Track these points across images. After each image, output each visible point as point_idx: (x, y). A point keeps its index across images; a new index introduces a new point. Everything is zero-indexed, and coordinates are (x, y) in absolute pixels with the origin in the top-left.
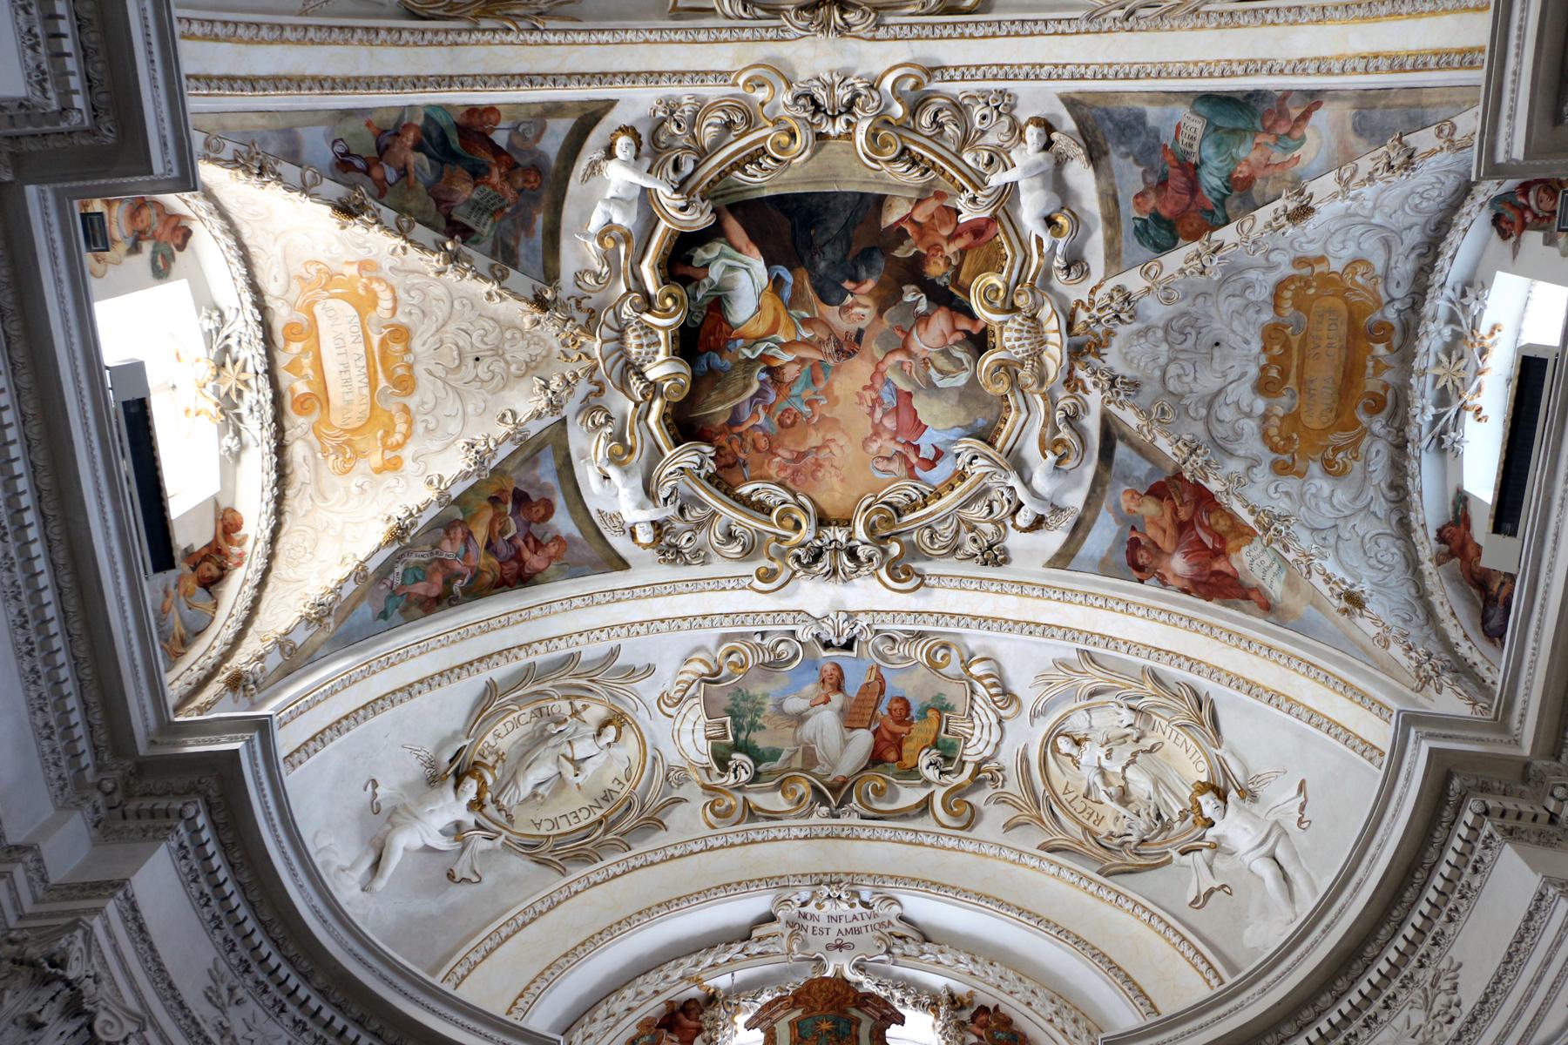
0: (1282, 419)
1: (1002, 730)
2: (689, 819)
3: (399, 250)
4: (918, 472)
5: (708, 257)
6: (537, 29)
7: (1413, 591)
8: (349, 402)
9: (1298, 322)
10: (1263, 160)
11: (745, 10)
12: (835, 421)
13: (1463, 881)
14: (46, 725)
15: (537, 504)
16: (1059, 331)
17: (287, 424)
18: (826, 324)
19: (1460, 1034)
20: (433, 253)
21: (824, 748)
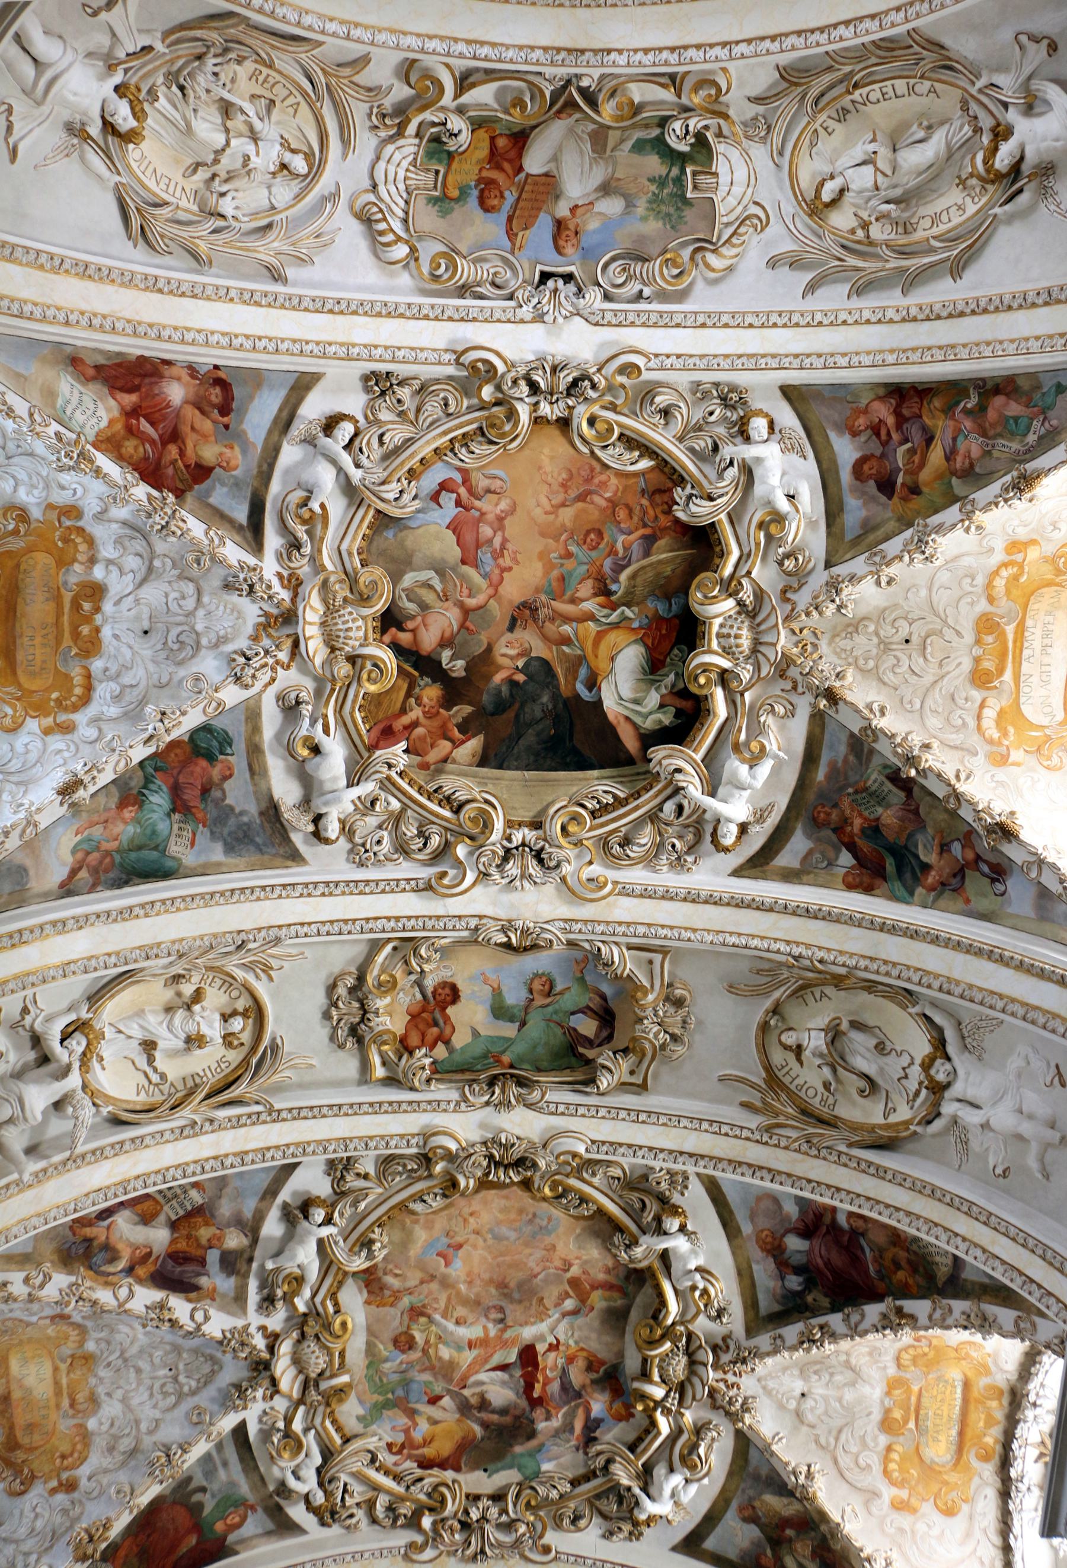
0: (74, 560)
1: (372, 177)
3: (963, 776)
4: (458, 477)
5: (659, 716)
6: (794, 957)
8: (1049, 613)
9: (66, 660)
10: (110, 826)
11: (599, 949)
12: (543, 535)
15: (870, 477)
16: (306, 640)
18: (545, 638)
20: (930, 768)
21: (581, 152)
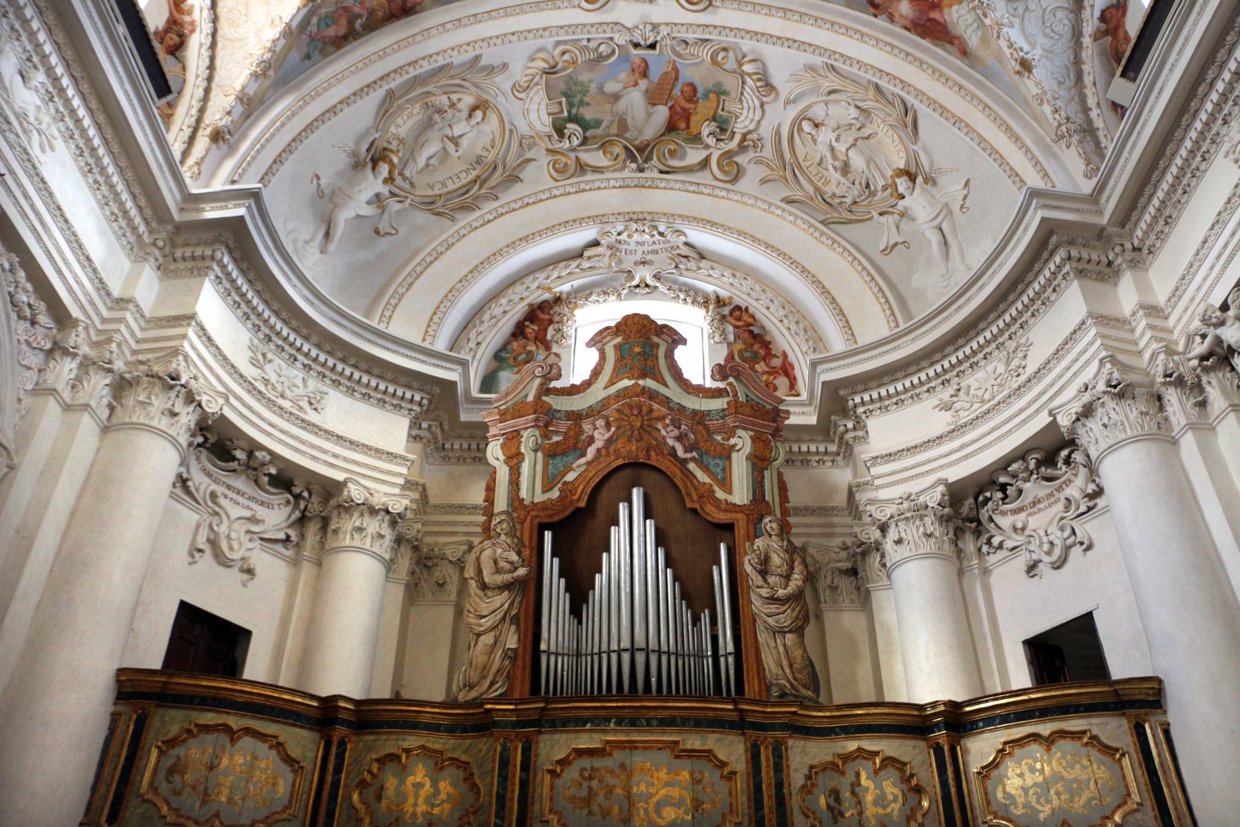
1: (763, 111)
2: (538, 174)
7: (1072, 57)
13: (1046, 295)
14: (112, 213)
19: (1020, 387)
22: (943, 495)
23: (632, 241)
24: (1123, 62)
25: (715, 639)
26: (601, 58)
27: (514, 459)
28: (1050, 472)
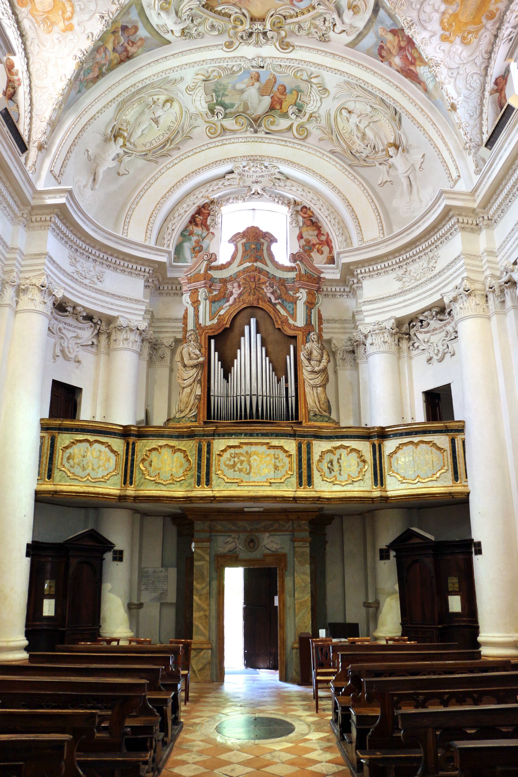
0: (451, 15)
7: (479, 101)
13: (447, 235)
15: (131, 29)
17: (18, 12)
21: (251, 103)
22: (393, 324)
23: (251, 171)
24: (503, 110)
25: (287, 389)
26: (234, 73)
27: (196, 303)
28: (441, 317)
